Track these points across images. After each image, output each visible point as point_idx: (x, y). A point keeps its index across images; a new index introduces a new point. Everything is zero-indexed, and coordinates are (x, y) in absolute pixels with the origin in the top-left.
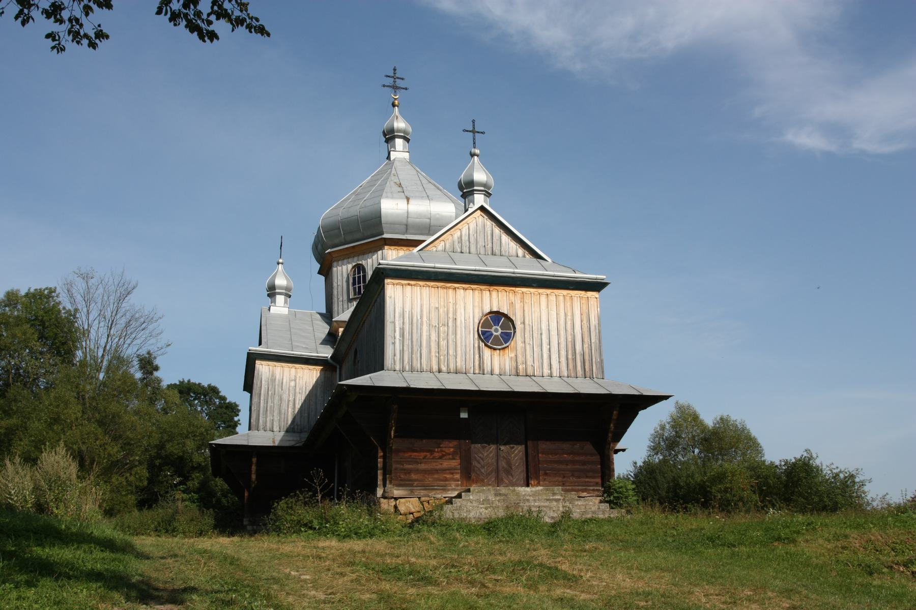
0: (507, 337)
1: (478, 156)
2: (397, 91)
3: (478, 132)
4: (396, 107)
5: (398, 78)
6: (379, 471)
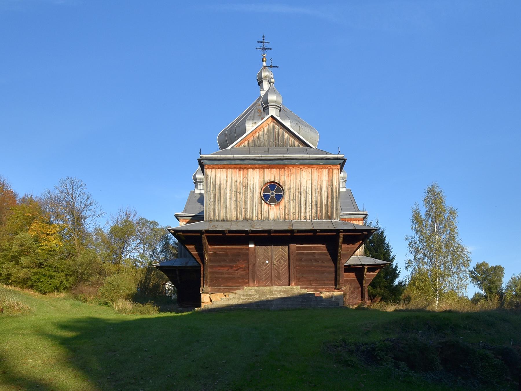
0: (279, 197)
1: (273, 83)
2: (265, 51)
3: (274, 67)
4: (265, 62)
5: (265, 42)
6: (201, 278)
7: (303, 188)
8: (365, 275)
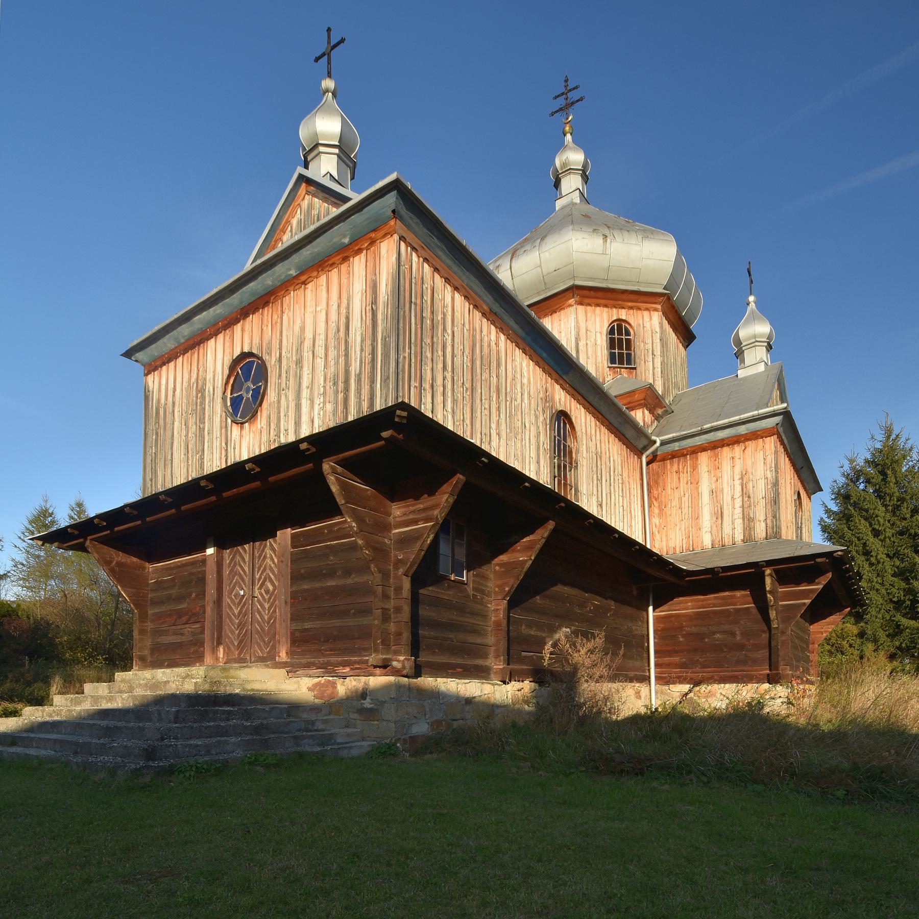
7: (308, 344)
8: (768, 595)
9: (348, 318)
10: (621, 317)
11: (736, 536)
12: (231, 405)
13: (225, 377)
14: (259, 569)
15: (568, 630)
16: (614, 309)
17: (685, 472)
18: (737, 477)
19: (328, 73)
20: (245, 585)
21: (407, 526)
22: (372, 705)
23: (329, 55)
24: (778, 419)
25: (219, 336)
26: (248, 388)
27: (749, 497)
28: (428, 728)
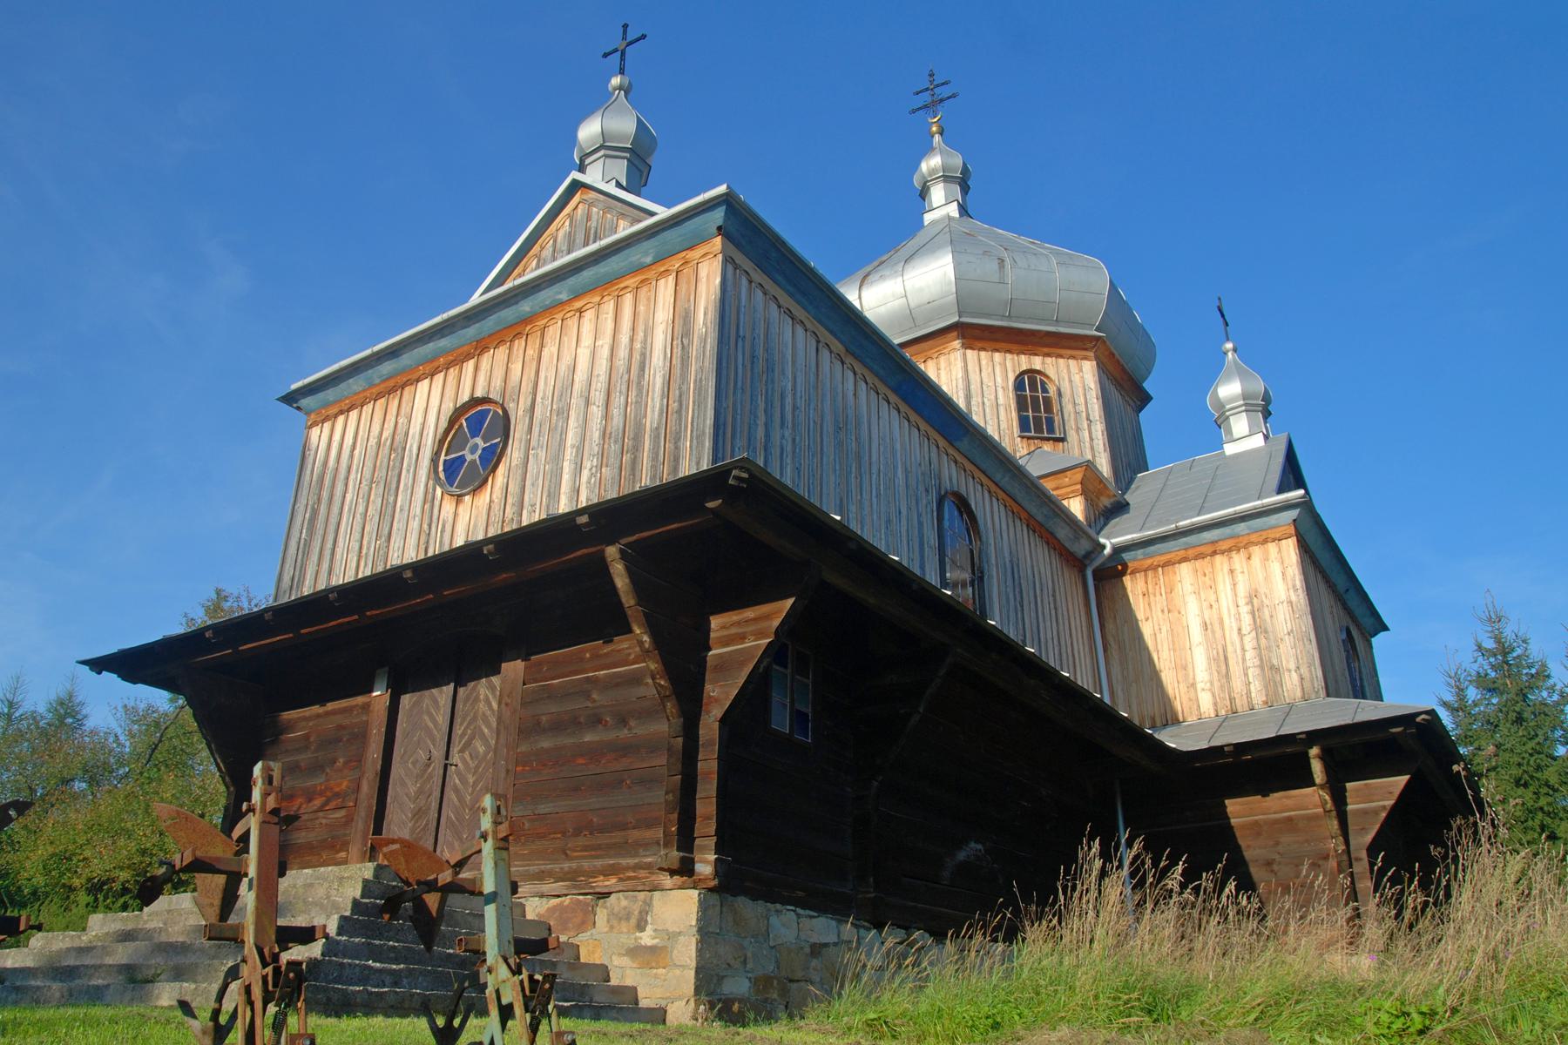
9: (643, 355)
10: (1033, 367)
11: (1253, 695)
12: (444, 470)
13: (441, 430)
14: (464, 719)
15: (980, 847)
16: (1023, 356)
17: (1158, 594)
18: (1242, 602)
19: (621, 69)
20: (434, 745)
21: (727, 645)
22: (657, 941)
23: (623, 53)
24: (1294, 513)
25: (436, 377)
26: (476, 446)
27: (1266, 632)
28: (750, 987)
